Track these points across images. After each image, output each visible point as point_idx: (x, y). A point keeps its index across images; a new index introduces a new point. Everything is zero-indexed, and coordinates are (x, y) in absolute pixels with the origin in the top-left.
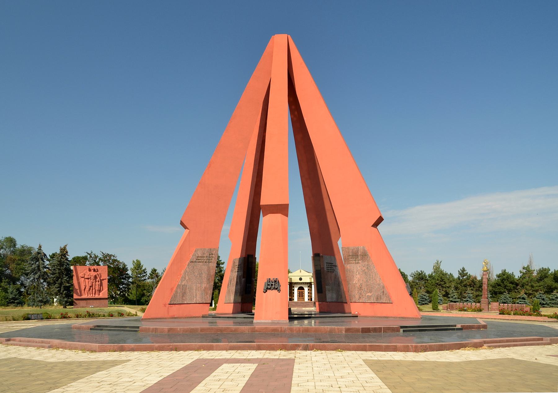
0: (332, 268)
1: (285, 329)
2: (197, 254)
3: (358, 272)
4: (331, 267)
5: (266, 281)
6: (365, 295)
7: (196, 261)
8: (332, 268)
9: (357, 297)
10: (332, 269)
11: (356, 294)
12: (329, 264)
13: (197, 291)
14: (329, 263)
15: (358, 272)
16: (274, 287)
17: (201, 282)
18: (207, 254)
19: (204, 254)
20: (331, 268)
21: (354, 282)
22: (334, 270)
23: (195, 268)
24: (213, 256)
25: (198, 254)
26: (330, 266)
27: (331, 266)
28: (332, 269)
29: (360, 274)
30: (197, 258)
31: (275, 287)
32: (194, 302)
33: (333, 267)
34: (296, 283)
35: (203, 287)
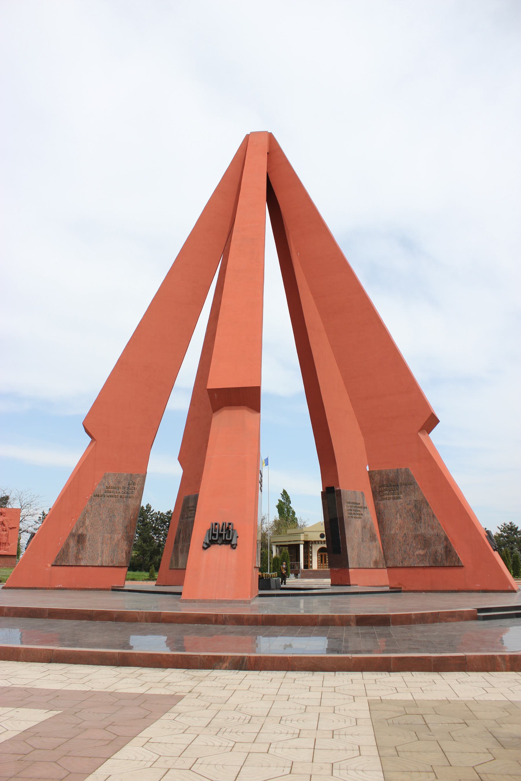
1: (225, 618)
2: (106, 483)
3: (398, 514)
4: (355, 509)
5: (209, 526)
6: (414, 554)
7: (105, 494)
9: (399, 557)
10: (359, 512)
11: (396, 552)
12: (351, 505)
13: (104, 545)
14: (353, 503)
15: (398, 514)
16: (224, 539)
17: (112, 531)
18: (124, 483)
19: (119, 482)
20: (356, 511)
21: (392, 532)
22: (362, 514)
23: (102, 507)
24: (136, 486)
25: (109, 484)
26: (352, 509)
27: (356, 507)
29: (402, 517)
30: (106, 490)
31: (227, 539)
32: (99, 563)
33: (359, 509)
34: (315, 542)
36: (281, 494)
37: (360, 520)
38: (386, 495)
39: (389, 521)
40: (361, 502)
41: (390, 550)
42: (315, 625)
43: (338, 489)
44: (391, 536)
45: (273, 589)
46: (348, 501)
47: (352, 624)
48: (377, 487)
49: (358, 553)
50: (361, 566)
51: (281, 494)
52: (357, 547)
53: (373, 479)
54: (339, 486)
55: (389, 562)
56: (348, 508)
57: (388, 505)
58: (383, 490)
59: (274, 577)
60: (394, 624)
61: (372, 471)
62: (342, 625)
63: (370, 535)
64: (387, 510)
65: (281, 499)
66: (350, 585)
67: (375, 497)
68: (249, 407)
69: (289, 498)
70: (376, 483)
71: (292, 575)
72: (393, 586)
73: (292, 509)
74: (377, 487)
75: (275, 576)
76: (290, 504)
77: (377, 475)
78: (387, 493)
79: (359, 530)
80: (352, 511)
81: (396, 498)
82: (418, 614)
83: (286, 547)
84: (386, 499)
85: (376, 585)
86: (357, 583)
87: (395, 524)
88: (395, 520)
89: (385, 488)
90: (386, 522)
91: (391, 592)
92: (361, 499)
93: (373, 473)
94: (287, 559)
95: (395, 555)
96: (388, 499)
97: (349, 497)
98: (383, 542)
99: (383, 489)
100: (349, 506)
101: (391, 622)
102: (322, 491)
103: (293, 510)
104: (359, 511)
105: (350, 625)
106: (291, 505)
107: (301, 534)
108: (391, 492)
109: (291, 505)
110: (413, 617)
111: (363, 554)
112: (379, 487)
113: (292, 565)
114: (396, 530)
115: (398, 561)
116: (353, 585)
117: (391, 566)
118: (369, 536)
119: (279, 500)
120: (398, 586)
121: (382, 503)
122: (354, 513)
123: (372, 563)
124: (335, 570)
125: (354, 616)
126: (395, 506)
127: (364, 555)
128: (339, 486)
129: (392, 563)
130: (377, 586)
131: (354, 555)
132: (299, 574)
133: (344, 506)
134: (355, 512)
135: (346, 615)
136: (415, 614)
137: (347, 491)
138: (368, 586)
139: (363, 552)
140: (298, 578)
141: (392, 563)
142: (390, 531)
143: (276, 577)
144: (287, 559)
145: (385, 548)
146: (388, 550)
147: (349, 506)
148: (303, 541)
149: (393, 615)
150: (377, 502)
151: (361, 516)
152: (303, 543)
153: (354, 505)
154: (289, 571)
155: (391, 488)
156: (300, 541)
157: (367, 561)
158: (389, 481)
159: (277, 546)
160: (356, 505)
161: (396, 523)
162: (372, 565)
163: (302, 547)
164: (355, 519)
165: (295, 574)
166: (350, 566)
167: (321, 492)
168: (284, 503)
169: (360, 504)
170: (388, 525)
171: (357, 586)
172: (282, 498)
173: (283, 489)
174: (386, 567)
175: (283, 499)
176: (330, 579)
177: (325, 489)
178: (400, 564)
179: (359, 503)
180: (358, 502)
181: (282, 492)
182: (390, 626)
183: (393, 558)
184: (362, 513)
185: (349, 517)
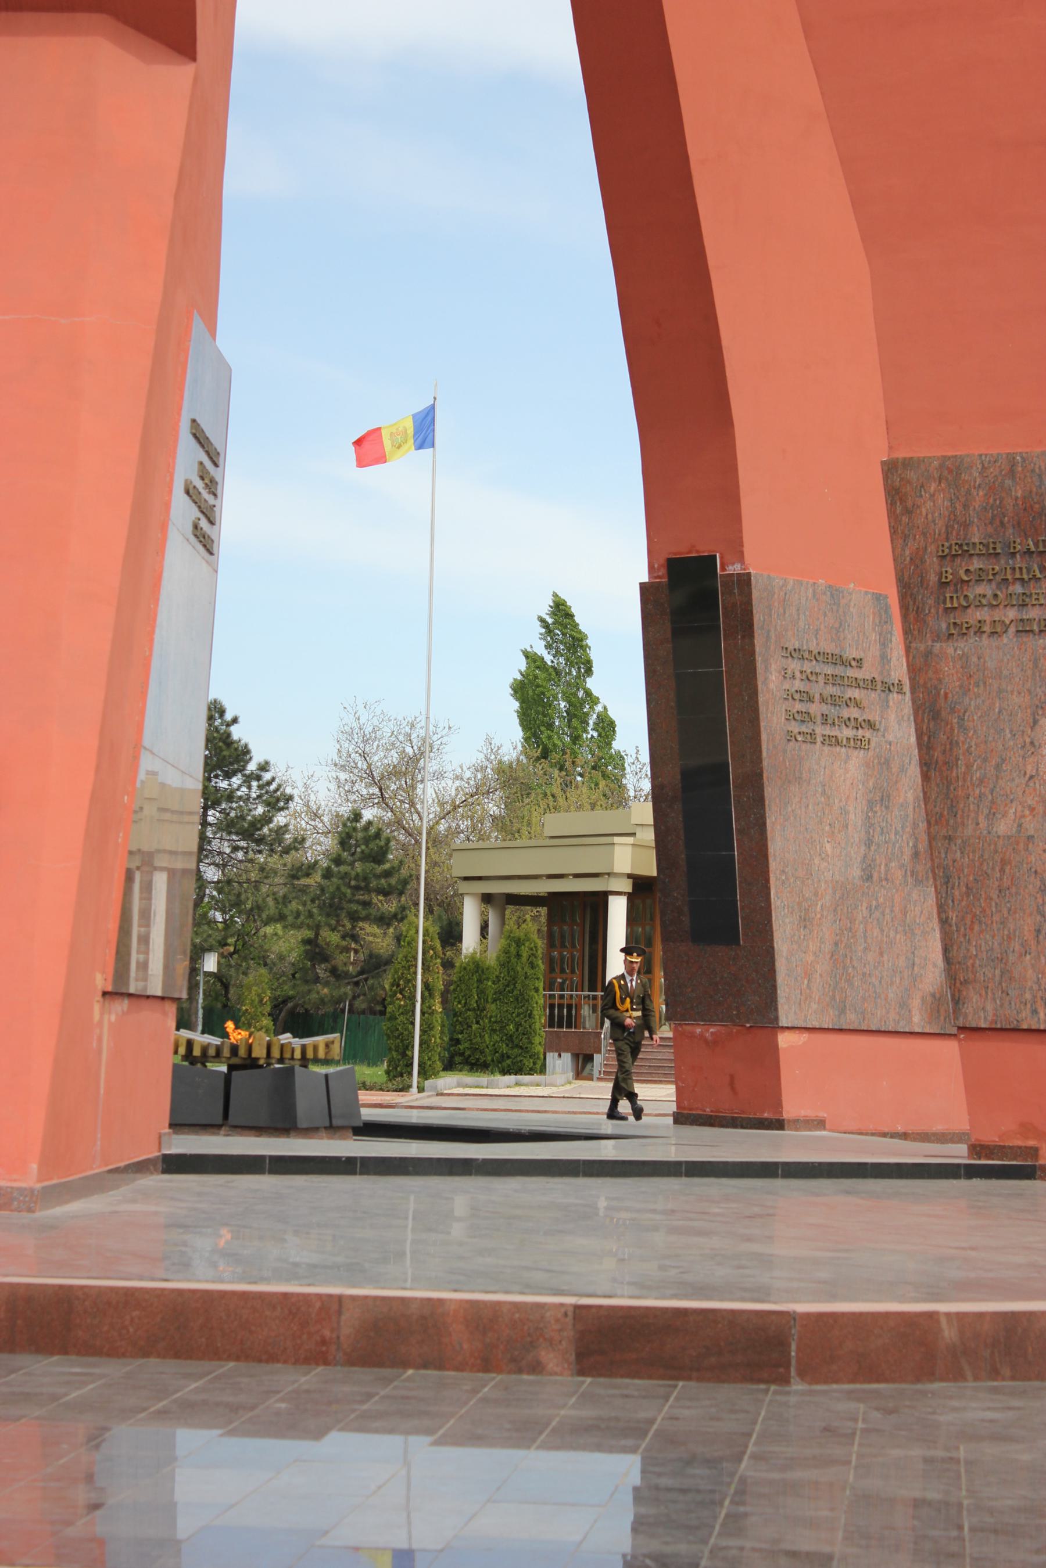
0: (849, 702)
8: (849, 702)
10: (854, 713)
12: (808, 667)
14: (819, 656)
20: (834, 701)
21: (1003, 827)
22: (871, 725)
26: (817, 689)
28: (854, 713)
33: (855, 693)
35: (854, 758)
36: (542, 620)
37: (857, 758)
38: (981, 605)
39: (985, 760)
40: (871, 654)
41: (981, 932)
42: (319, 1356)
43: (734, 569)
44: (996, 852)
45: (310, 1131)
46: (793, 643)
47: (550, 1358)
48: (932, 562)
49: (836, 944)
50: (851, 1020)
51: (542, 620)
52: (835, 910)
53: (908, 511)
54: (742, 553)
55: (975, 998)
56: (787, 687)
57: (989, 664)
58: (966, 578)
59: (316, 1061)
60: (811, 1372)
61: (907, 463)
62: (486, 1364)
63: (915, 846)
64: (977, 696)
65: (540, 648)
66: (779, 1124)
67: (912, 617)
68: (126, 22)
69: (585, 648)
70: (924, 534)
71: (559, 1062)
72: (990, 1137)
73: (599, 708)
74: (932, 562)
75: (326, 1054)
76: (588, 680)
77: (933, 486)
78: (989, 593)
79: (847, 813)
80: (811, 700)
81: (1035, 628)
82: (981, 1315)
83: (540, 905)
84: (979, 632)
85: (939, 1127)
86: (822, 1114)
87: (1024, 781)
88: (1023, 757)
89: (976, 564)
90: (969, 766)
91: (971, 1172)
92: (874, 636)
93: (912, 475)
94: (530, 972)
95: (1012, 958)
96: (987, 628)
97: (801, 624)
98: (947, 883)
99: (962, 573)
100: (798, 675)
101: (793, 1362)
102: (645, 579)
103: (605, 708)
104: (857, 705)
105: (536, 1368)
106: (591, 683)
107: (617, 840)
108: (1011, 589)
109: (591, 683)
110: (949, 1333)
111: (866, 949)
112: (943, 557)
113: (561, 1006)
114: (1027, 812)
115: (1028, 996)
116: (796, 1121)
117: (983, 1026)
118: (908, 852)
119: (527, 655)
120: (1019, 1142)
121: (950, 651)
122: (825, 717)
123: (916, 1003)
124: (701, 1035)
125: (566, 1315)
126: (1029, 672)
127: (871, 957)
128: (740, 557)
129: (989, 1007)
130: (925, 1137)
131: (810, 958)
132: (597, 1058)
133: (767, 669)
134: (832, 712)
135: (516, 1305)
136: (961, 1316)
137: (789, 587)
138: (884, 1135)
139: (865, 937)
140: (590, 1078)
141: (989, 1007)
142: (991, 816)
143: (338, 1063)
144: (530, 972)
145: (953, 916)
146: (971, 929)
147: (798, 675)
148: (629, 876)
149: (808, 1315)
150: (922, 647)
151: (868, 734)
152: (627, 886)
153: (829, 670)
154: (537, 1040)
155: (1014, 569)
156: (609, 874)
157: (891, 995)
158: (1002, 523)
159: (487, 899)
160: (839, 670)
161: (1030, 770)
162: (916, 1019)
163: (618, 911)
164: (826, 748)
165: (576, 1056)
166: (786, 1016)
167: (643, 587)
168: (558, 672)
169: (866, 665)
170: (981, 781)
171: (824, 1133)
172: (543, 643)
173: (555, 595)
174: (954, 1031)
175: (548, 647)
176: (674, 1087)
177: (663, 572)
178: (1035, 1012)
179: (859, 661)
180: (850, 653)
181: (544, 608)
182: (785, 1380)
183: (997, 978)
184: (874, 716)
185: (791, 737)
